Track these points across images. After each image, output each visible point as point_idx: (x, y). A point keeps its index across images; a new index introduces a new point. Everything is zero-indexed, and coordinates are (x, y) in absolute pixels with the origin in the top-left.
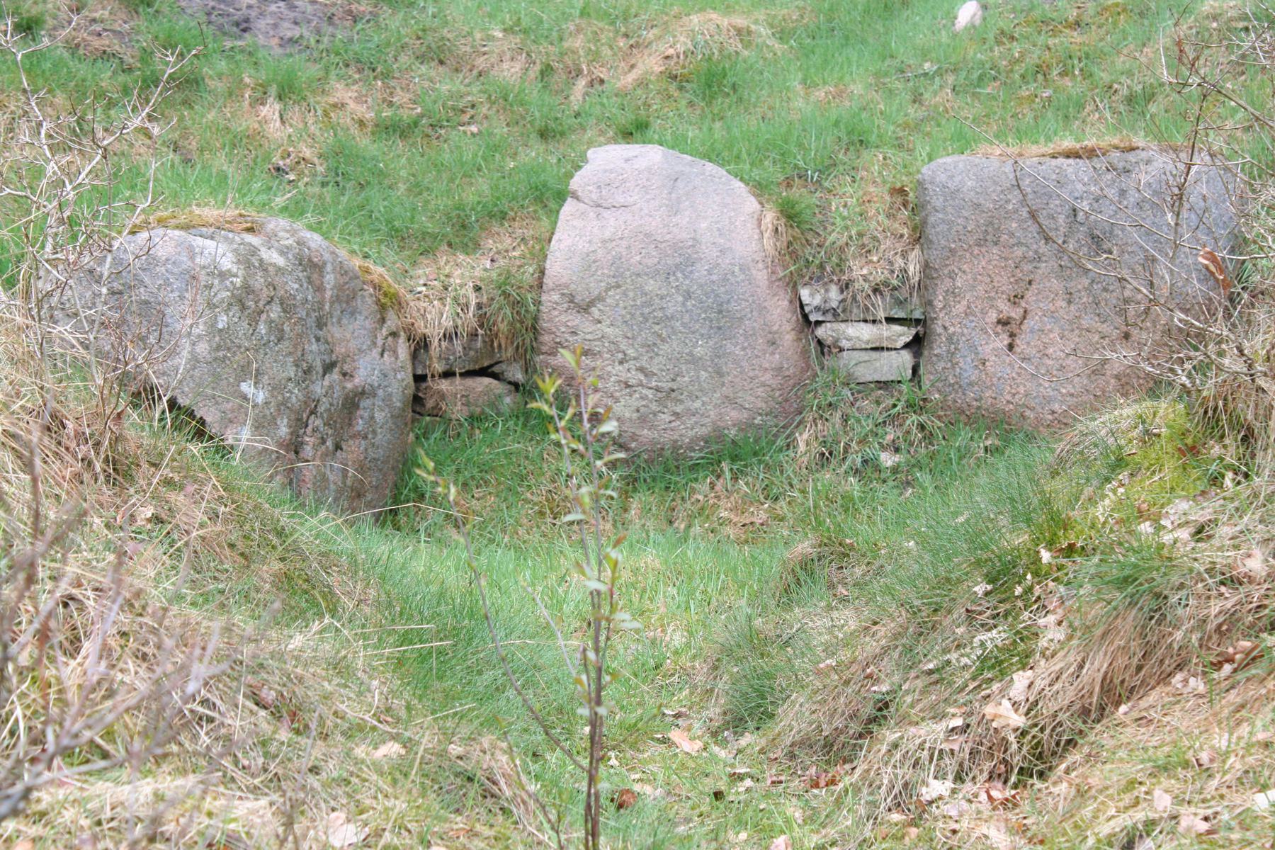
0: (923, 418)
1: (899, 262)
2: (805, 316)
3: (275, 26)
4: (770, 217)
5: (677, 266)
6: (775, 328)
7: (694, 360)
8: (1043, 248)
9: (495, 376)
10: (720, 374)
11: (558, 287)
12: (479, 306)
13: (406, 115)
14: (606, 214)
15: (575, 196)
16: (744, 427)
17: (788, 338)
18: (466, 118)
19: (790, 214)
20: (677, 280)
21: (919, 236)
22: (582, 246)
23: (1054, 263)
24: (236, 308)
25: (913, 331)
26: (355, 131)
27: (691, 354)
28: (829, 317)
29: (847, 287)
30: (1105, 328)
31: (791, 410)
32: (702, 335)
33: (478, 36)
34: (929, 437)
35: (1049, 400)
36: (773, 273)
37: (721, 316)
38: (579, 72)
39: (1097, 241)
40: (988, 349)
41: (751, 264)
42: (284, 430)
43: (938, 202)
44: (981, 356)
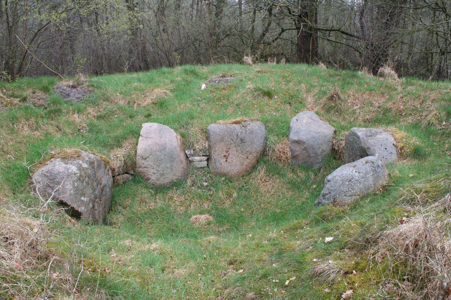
0: (210, 175)
1: (204, 144)
2: (187, 156)
3: (74, 95)
7: (167, 168)
8: (232, 142)
9: (128, 173)
10: (172, 170)
11: (139, 155)
12: (124, 160)
13: (103, 114)
14: (148, 139)
15: (142, 136)
17: (184, 161)
18: (114, 114)
19: (183, 136)
21: (208, 138)
22: (144, 147)
24: (79, 181)
26: (93, 118)
30: (243, 156)
31: (186, 175)
33: (115, 95)
34: (212, 178)
37: (172, 158)
38: (135, 102)
39: (242, 140)
42: (91, 205)
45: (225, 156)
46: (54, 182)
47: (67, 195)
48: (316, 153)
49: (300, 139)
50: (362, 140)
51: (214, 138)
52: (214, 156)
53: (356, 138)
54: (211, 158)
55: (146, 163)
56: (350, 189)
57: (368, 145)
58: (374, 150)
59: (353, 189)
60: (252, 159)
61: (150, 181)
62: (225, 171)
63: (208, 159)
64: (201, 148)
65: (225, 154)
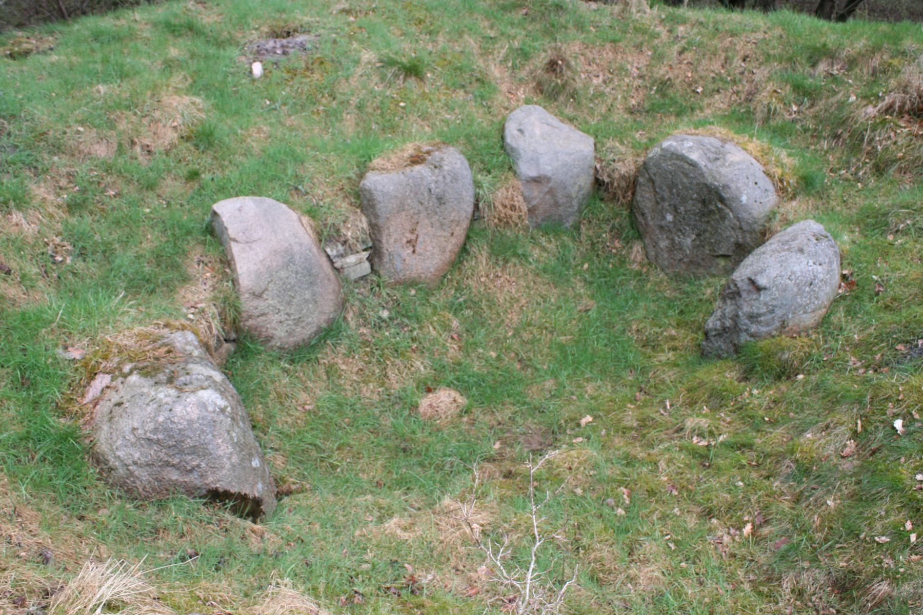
7: (306, 301)
8: (421, 208)
14: (254, 246)
15: (235, 240)
16: (327, 321)
19: (312, 213)
22: (253, 268)
23: (425, 213)
35: (429, 268)
39: (440, 200)
43: (380, 199)
45: (409, 242)
46: (181, 452)
47: (224, 472)
48: (569, 196)
49: (541, 172)
50: (704, 169)
51: (386, 207)
53: (686, 166)
55: (261, 305)
56: (813, 299)
57: (723, 181)
58: (738, 189)
59: (817, 298)
60: (460, 231)
61: (273, 343)
62: (414, 275)
65: (410, 236)
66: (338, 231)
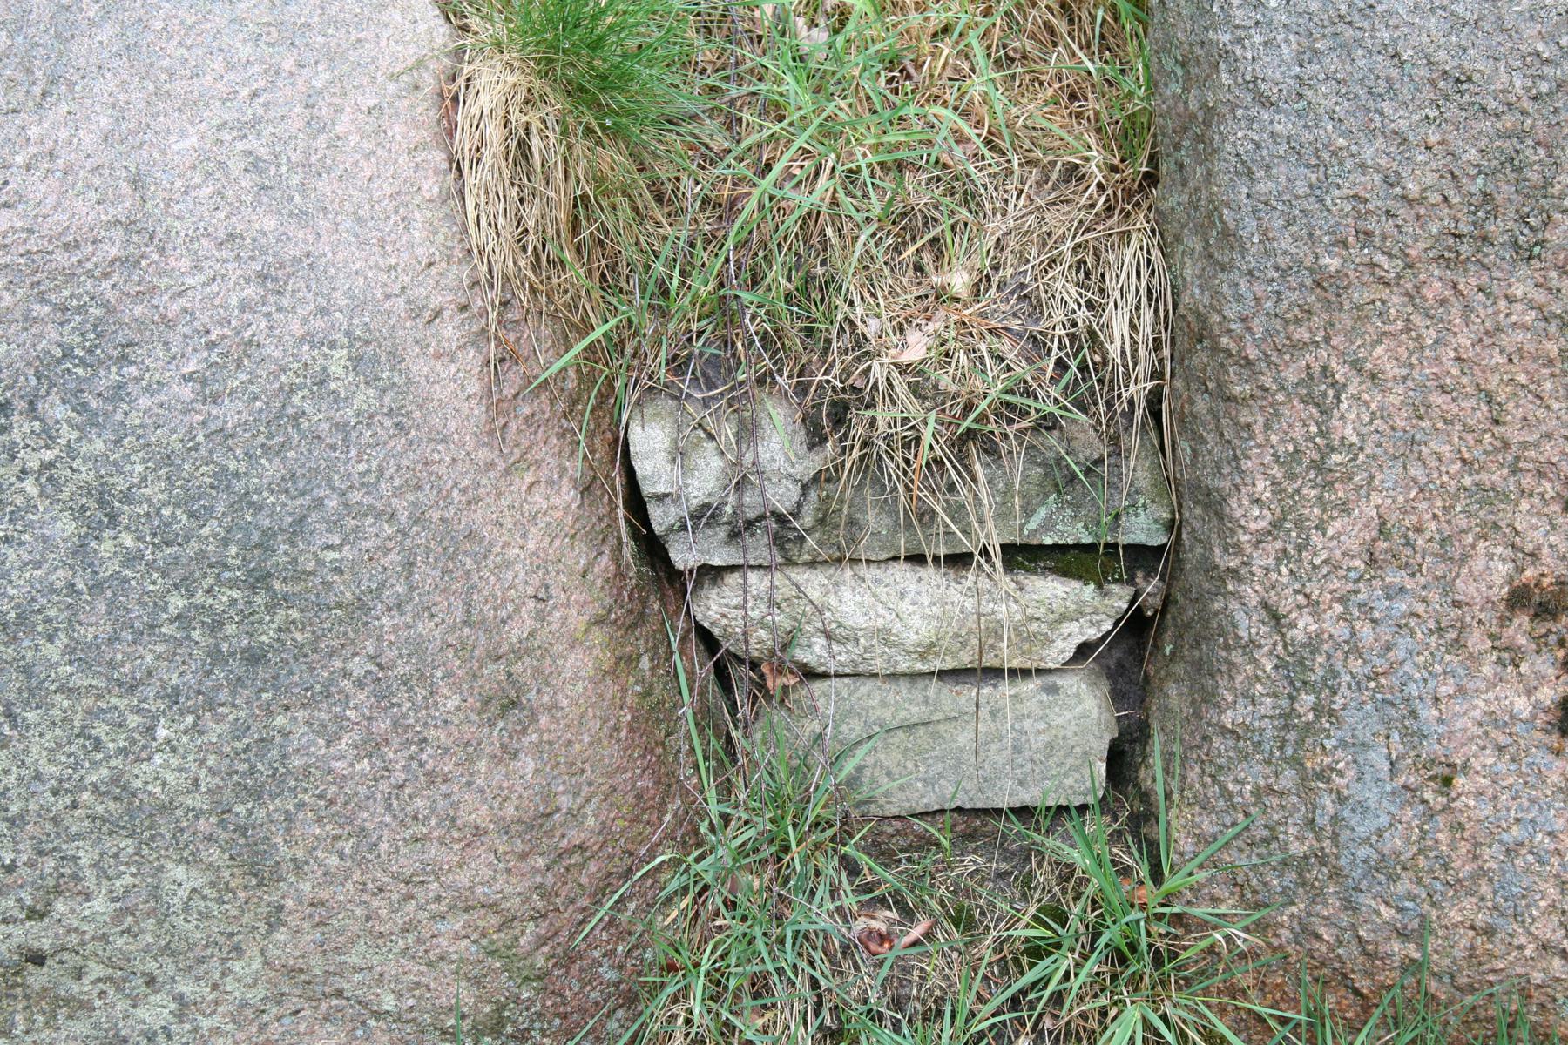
2: (652, 548)
4: (494, 85)
5: (46, 368)
6: (516, 632)
7: (135, 816)
10: (259, 868)
17: (577, 669)
20: (48, 436)
21: (1152, 166)
25: (1119, 599)
27: (118, 787)
28: (759, 547)
29: (839, 416)
32: (174, 696)
36: (508, 357)
37: (256, 593)
40: (1466, 717)
41: (409, 332)
44: (1430, 748)
51: (1319, 160)
52: (1287, 580)
54: (1209, 633)
63: (1137, 628)
64: (992, 386)
66: (814, 290)
